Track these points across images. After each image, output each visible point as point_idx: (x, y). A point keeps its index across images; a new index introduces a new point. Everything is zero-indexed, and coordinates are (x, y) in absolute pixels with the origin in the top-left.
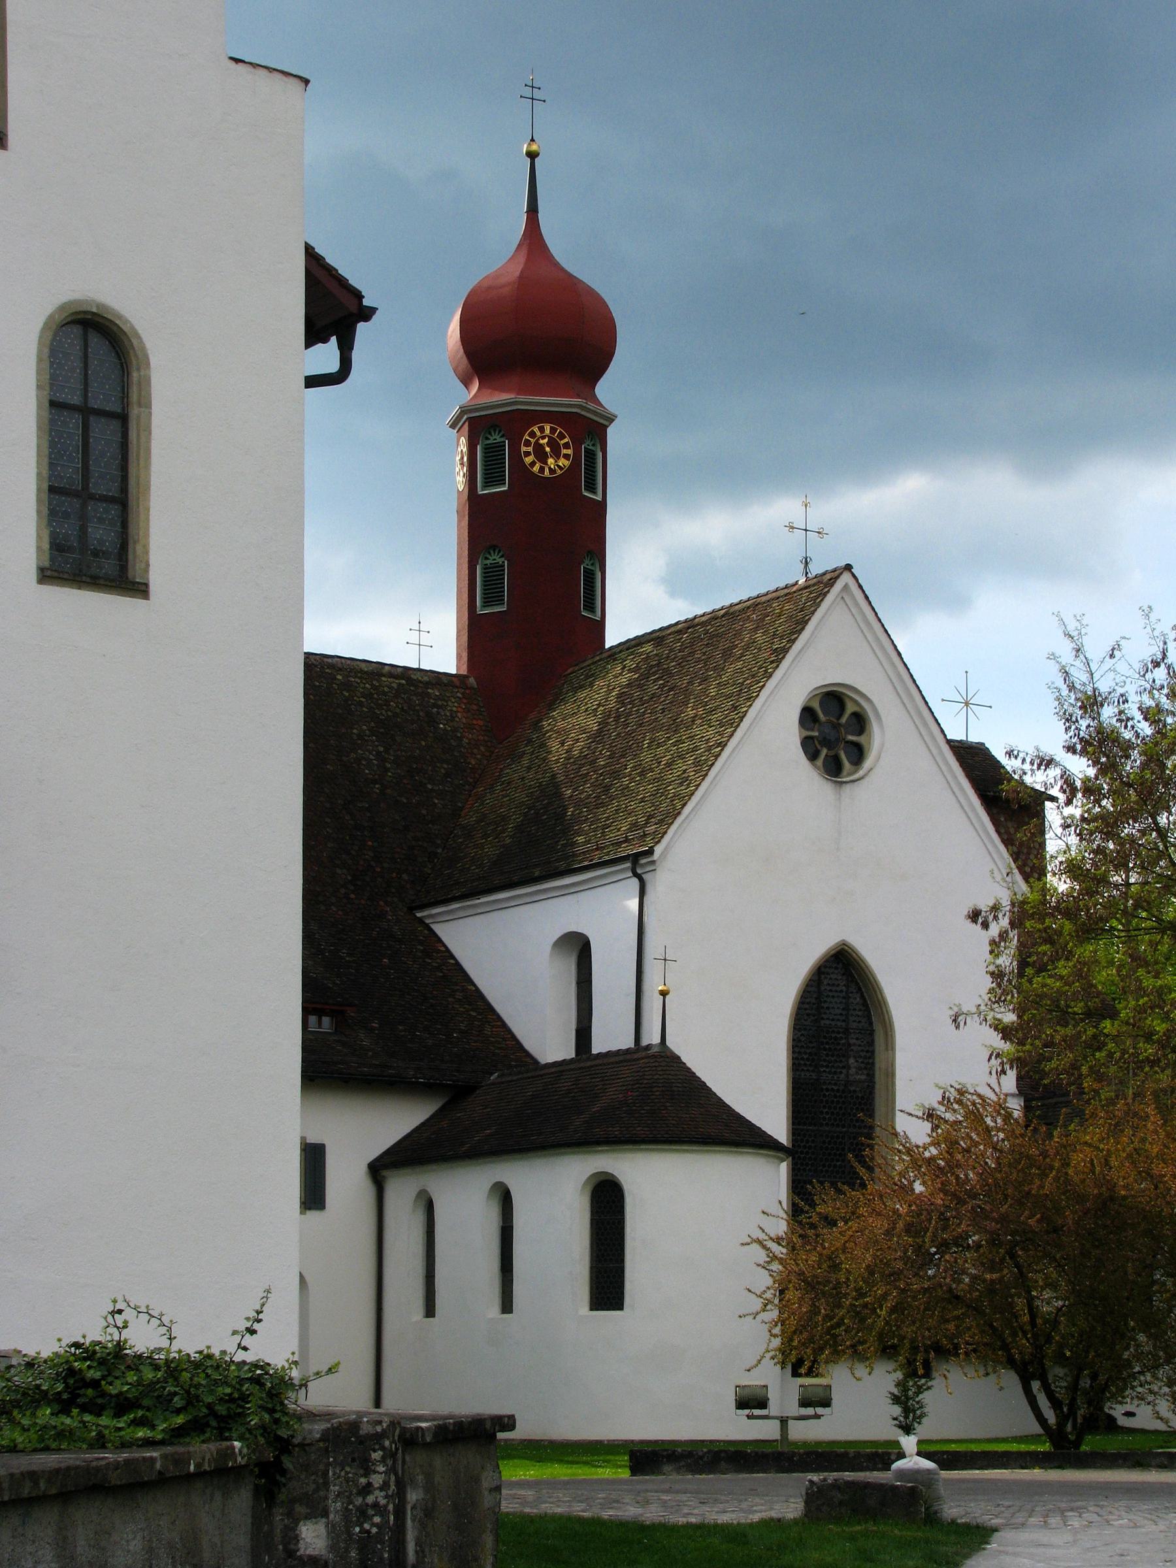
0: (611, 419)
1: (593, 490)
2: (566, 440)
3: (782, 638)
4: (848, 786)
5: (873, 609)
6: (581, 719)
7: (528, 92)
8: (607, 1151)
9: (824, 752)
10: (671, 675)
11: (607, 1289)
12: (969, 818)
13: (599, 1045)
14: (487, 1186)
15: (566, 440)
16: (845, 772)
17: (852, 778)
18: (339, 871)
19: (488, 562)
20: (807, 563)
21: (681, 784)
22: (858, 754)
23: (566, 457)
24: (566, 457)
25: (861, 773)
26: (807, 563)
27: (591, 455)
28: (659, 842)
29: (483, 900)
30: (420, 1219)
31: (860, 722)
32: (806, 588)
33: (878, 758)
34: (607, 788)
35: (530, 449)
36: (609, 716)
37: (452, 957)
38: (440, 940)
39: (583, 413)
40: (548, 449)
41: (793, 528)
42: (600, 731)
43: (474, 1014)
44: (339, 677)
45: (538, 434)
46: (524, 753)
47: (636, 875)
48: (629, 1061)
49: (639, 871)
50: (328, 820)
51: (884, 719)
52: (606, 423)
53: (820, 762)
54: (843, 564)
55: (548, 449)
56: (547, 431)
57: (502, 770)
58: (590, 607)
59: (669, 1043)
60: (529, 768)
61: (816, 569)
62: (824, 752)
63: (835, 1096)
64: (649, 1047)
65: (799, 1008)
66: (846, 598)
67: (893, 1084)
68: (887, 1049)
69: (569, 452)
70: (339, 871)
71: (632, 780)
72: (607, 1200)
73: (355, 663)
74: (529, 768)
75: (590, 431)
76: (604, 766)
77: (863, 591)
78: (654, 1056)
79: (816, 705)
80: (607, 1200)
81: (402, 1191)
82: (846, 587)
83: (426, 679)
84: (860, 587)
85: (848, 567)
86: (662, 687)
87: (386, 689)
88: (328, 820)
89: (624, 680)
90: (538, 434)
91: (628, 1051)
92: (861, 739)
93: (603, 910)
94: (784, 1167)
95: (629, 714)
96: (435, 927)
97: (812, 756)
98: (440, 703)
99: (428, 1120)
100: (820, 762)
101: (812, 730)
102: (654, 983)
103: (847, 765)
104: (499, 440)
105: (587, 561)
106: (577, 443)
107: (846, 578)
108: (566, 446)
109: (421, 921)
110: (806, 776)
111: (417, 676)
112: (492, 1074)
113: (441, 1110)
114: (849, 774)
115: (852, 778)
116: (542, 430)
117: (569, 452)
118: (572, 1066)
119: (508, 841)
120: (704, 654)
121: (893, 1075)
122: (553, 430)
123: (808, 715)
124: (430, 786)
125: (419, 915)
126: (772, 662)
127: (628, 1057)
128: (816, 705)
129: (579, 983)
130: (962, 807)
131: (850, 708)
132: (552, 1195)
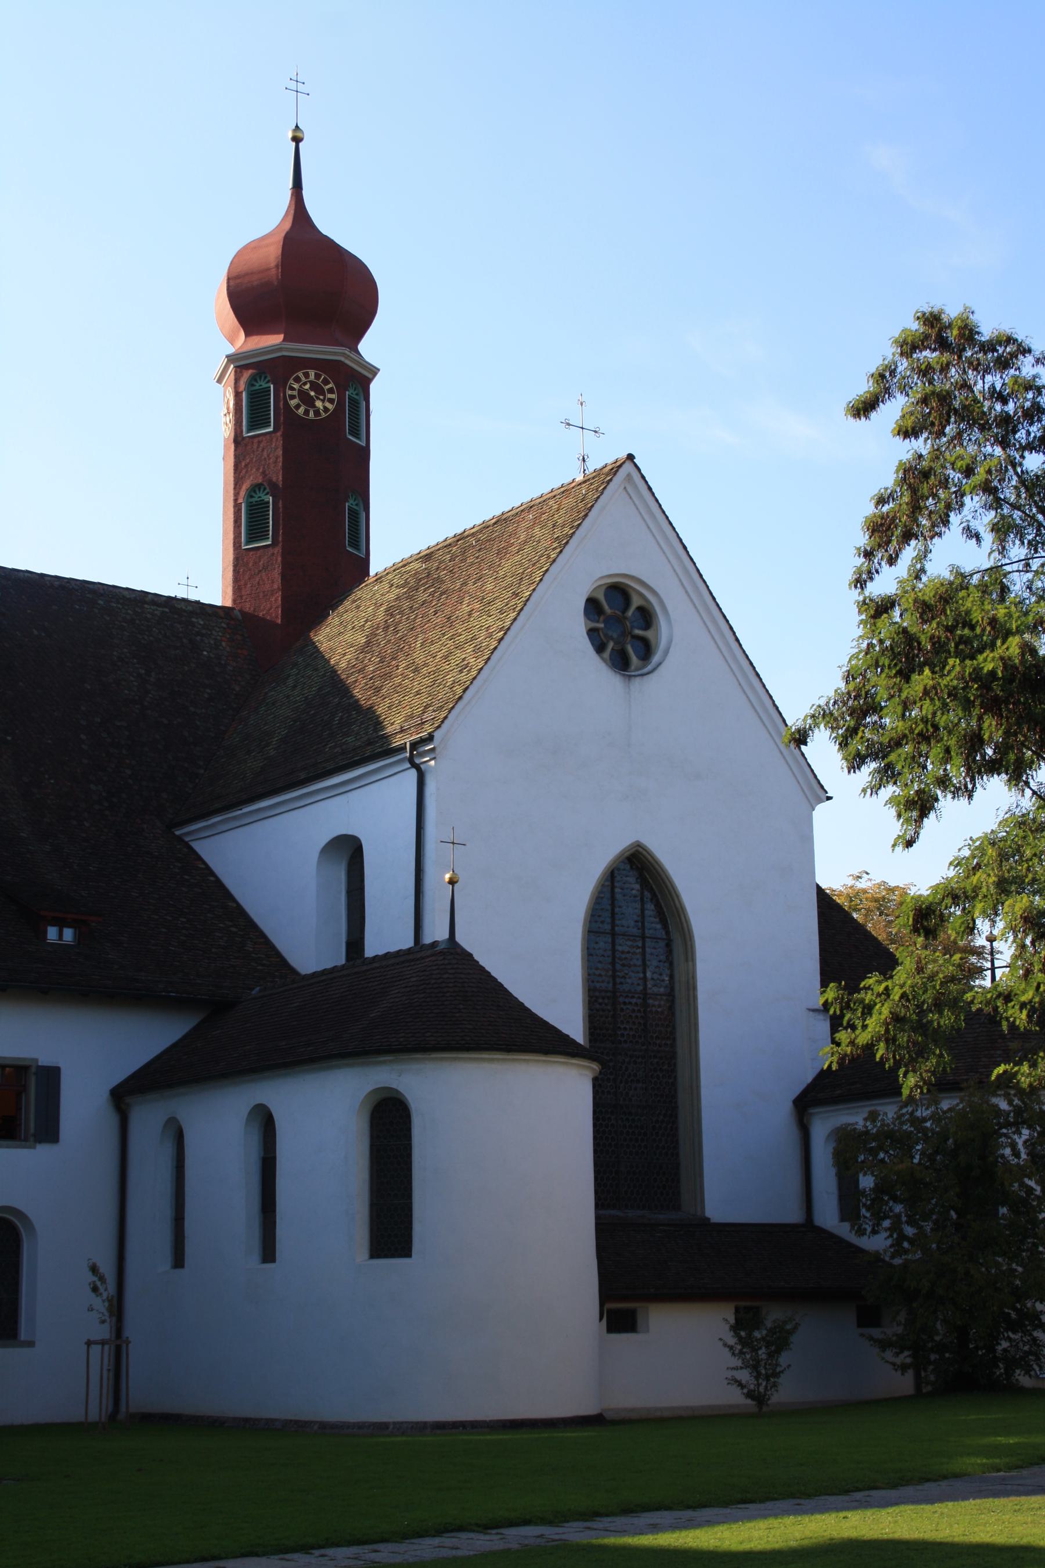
0: (374, 371)
1: (357, 435)
2: (330, 386)
3: (563, 526)
4: (638, 679)
5: (657, 501)
6: (348, 636)
7: (293, 85)
8: (390, 1061)
9: (611, 645)
10: (443, 582)
11: (391, 1227)
12: (760, 717)
13: (373, 947)
14: (245, 1111)
15: (330, 386)
16: (633, 668)
17: (640, 672)
18: (93, 787)
19: (253, 500)
20: (584, 460)
21: (461, 671)
22: (646, 649)
23: (331, 401)
24: (331, 401)
25: (649, 668)
26: (584, 460)
27: (355, 404)
28: (439, 727)
29: (245, 810)
30: (168, 1151)
31: (647, 616)
32: (585, 482)
33: (667, 652)
34: (378, 690)
35: (295, 393)
36: (377, 628)
37: (212, 873)
38: (200, 858)
39: (347, 362)
40: (312, 393)
41: (569, 424)
42: (368, 643)
43: (234, 929)
44: (101, 602)
45: (304, 379)
46: (289, 675)
47: (417, 767)
48: (413, 960)
49: (417, 761)
50: (83, 737)
51: (671, 613)
52: (370, 376)
53: (607, 654)
54: (623, 455)
55: (312, 393)
56: (312, 377)
57: (266, 693)
58: (355, 544)
59: (459, 938)
60: (294, 687)
61: (593, 465)
62: (611, 645)
63: (633, 1011)
64: (435, 944)
65: (592, 916)
66: (629, 489)
67: (695, 998)
68: (687, 960)
69: (333, 396)
70: (93, 787)
71: (405, 677)
72: (390, 1126)
73: (117, 590)
74: (294, 687)
75: (357, 381)
76: (374, 671)
77: (646, 482)
78: (441, 953)
79: (601, 597)
80: (390, 1126)
81: (148, 1118)
82: (629, 475)
83: (190, 608)
84: (643, 477)
85: (631, 457)
86: (432, 594)
87: (149, 616)
88: (83, 737)
89: (392, 596)
90: (304, 379)
91: (409, 951)
92: (649, 634)
93: (373, 807)
94: (408, 943)
95: (400, 622)
96: (195, 845)
97: (600, 649)
98: (204, 631)
99: (181, 1040)
100: (607, 654)
101: (598, 622)
102: (437, 877)
103: (634, 660)
104: (265, 386)
105: (351, 501)
106: (341, 389)
107: (628, 467)
108: (331, 391)
109: (180, 839)
110: (594, 670)
111: (182, 606)
112: (252, 989)
113: (195, 1029)
114: (637, 669)
115: (640, 672)
116: (307, 375)
117: (333, 396)
118: (345, 972)
119: (272, 753)
120: (477, 558)
121: (695, 988)
122: (317, 376)
123: (592, 606)
124: (192, 709)
125: (178, 833)
126: (554, 549)
127: (411, 957)
128: (601, 597)
129: (349, 892)
130: (754, 707)
131: (636, 602)
132: (322, 1115)
